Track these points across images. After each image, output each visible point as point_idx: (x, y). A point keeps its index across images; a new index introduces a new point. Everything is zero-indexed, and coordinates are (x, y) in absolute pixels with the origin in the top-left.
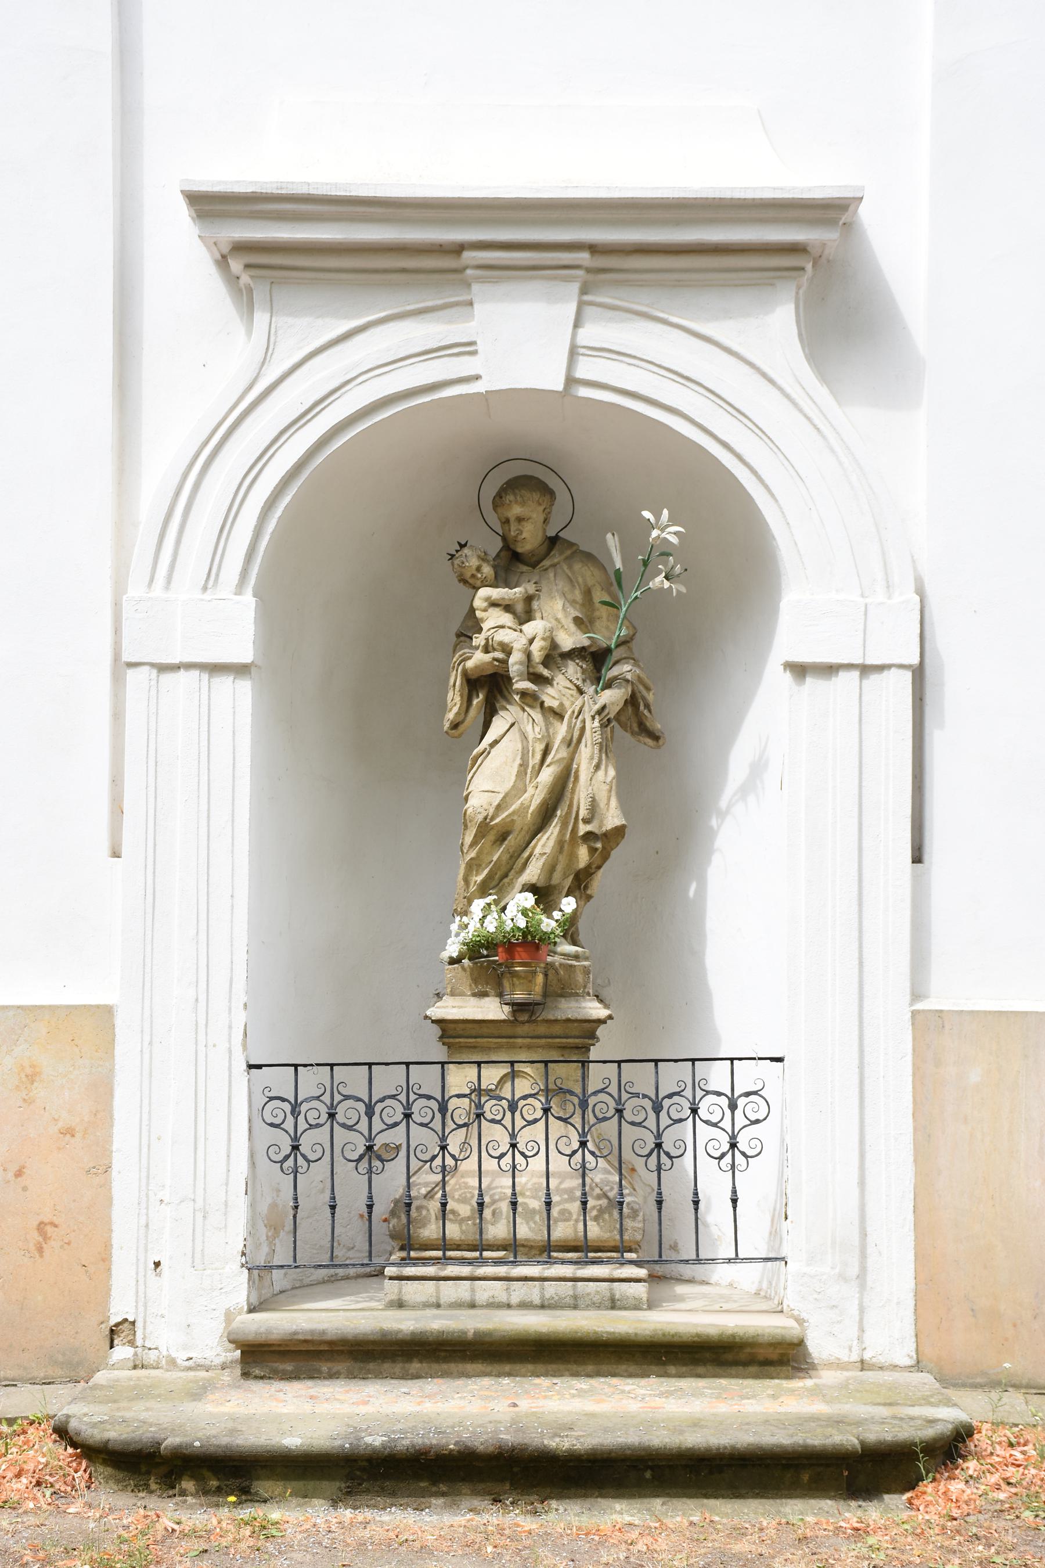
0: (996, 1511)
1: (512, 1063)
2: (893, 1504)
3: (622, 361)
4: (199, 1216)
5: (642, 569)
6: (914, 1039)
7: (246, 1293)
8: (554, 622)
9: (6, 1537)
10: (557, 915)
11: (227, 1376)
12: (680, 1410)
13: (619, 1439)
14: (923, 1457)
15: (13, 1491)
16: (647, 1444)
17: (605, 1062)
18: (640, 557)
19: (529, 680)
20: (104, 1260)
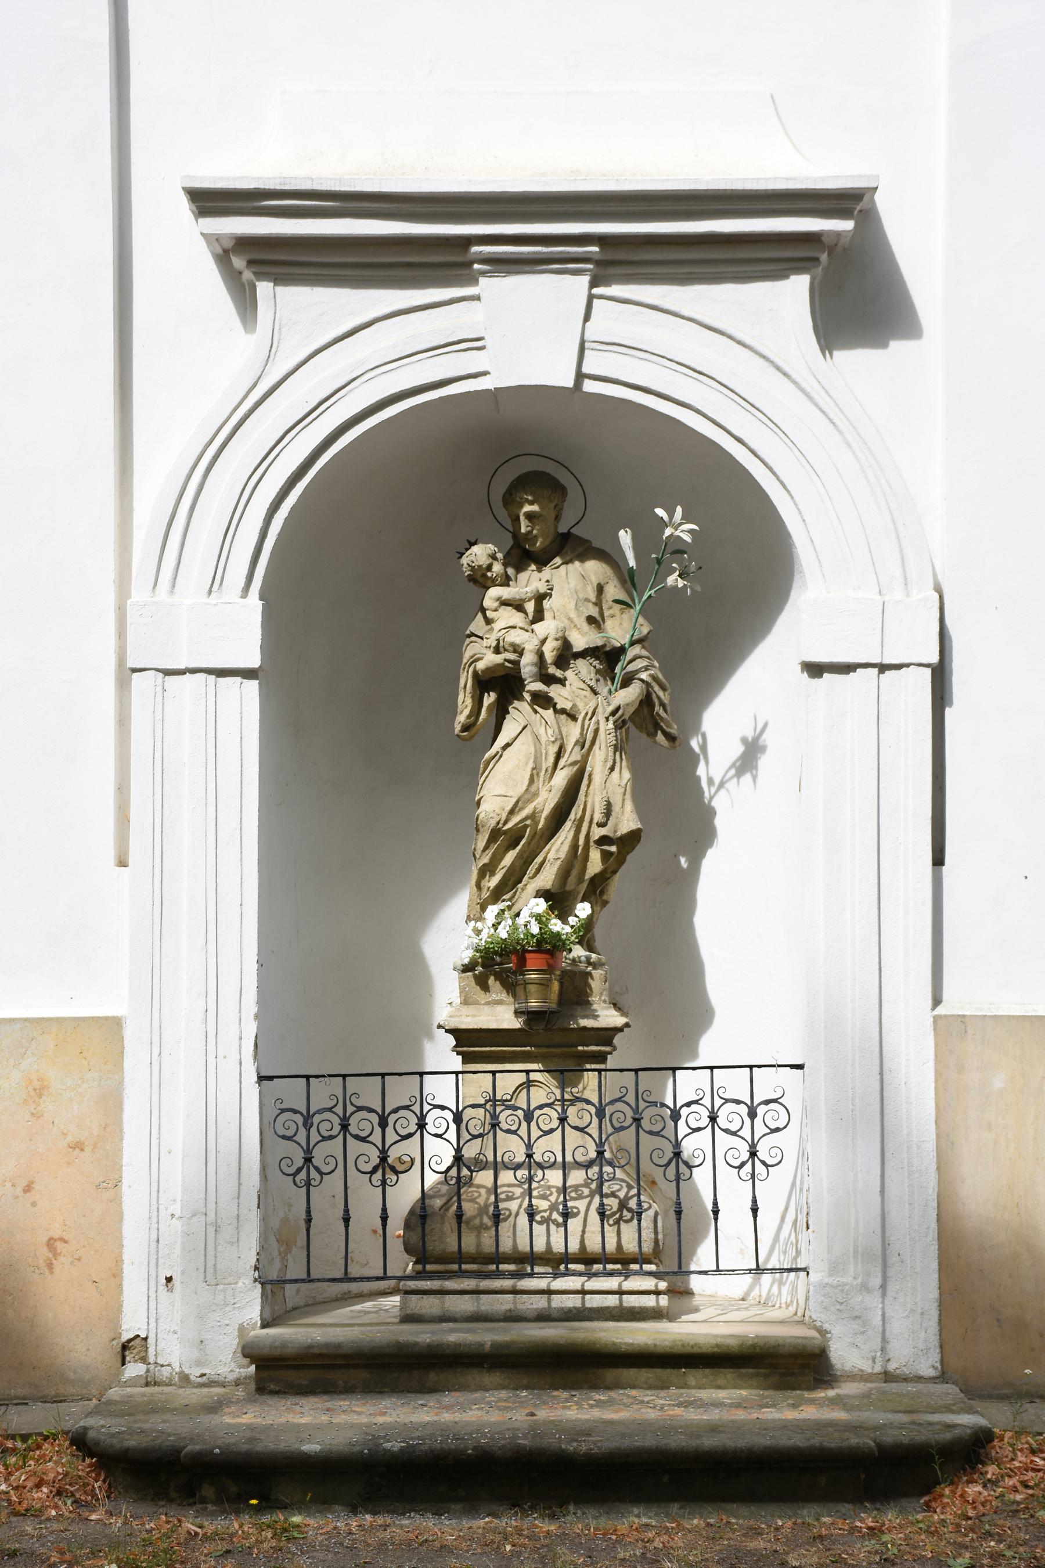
0: (1011, 1511)
1: (528, 1072)
2: (910, 1507)
3: (633, 356)
4: (211, 1230)
5: (657, 567)
6: (936, 1045)
7: (260, 1308)
8: (567, 622)
9: (31, 1541)
10: (572, 920)
11: (242, 1391)
12: (699, 1417)
13: (636, 1443)
14: (939, 1459)
15: (34, 1500)
16: (664, 1447)
17: (621, 1070)
18: (654, 556)
19: (542, 681)
20: (115, 1276)
